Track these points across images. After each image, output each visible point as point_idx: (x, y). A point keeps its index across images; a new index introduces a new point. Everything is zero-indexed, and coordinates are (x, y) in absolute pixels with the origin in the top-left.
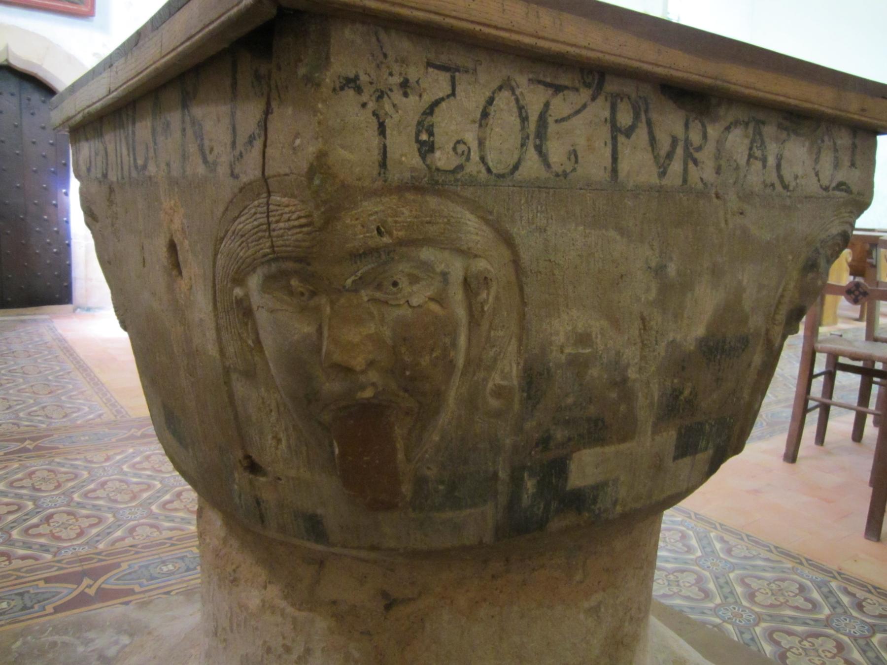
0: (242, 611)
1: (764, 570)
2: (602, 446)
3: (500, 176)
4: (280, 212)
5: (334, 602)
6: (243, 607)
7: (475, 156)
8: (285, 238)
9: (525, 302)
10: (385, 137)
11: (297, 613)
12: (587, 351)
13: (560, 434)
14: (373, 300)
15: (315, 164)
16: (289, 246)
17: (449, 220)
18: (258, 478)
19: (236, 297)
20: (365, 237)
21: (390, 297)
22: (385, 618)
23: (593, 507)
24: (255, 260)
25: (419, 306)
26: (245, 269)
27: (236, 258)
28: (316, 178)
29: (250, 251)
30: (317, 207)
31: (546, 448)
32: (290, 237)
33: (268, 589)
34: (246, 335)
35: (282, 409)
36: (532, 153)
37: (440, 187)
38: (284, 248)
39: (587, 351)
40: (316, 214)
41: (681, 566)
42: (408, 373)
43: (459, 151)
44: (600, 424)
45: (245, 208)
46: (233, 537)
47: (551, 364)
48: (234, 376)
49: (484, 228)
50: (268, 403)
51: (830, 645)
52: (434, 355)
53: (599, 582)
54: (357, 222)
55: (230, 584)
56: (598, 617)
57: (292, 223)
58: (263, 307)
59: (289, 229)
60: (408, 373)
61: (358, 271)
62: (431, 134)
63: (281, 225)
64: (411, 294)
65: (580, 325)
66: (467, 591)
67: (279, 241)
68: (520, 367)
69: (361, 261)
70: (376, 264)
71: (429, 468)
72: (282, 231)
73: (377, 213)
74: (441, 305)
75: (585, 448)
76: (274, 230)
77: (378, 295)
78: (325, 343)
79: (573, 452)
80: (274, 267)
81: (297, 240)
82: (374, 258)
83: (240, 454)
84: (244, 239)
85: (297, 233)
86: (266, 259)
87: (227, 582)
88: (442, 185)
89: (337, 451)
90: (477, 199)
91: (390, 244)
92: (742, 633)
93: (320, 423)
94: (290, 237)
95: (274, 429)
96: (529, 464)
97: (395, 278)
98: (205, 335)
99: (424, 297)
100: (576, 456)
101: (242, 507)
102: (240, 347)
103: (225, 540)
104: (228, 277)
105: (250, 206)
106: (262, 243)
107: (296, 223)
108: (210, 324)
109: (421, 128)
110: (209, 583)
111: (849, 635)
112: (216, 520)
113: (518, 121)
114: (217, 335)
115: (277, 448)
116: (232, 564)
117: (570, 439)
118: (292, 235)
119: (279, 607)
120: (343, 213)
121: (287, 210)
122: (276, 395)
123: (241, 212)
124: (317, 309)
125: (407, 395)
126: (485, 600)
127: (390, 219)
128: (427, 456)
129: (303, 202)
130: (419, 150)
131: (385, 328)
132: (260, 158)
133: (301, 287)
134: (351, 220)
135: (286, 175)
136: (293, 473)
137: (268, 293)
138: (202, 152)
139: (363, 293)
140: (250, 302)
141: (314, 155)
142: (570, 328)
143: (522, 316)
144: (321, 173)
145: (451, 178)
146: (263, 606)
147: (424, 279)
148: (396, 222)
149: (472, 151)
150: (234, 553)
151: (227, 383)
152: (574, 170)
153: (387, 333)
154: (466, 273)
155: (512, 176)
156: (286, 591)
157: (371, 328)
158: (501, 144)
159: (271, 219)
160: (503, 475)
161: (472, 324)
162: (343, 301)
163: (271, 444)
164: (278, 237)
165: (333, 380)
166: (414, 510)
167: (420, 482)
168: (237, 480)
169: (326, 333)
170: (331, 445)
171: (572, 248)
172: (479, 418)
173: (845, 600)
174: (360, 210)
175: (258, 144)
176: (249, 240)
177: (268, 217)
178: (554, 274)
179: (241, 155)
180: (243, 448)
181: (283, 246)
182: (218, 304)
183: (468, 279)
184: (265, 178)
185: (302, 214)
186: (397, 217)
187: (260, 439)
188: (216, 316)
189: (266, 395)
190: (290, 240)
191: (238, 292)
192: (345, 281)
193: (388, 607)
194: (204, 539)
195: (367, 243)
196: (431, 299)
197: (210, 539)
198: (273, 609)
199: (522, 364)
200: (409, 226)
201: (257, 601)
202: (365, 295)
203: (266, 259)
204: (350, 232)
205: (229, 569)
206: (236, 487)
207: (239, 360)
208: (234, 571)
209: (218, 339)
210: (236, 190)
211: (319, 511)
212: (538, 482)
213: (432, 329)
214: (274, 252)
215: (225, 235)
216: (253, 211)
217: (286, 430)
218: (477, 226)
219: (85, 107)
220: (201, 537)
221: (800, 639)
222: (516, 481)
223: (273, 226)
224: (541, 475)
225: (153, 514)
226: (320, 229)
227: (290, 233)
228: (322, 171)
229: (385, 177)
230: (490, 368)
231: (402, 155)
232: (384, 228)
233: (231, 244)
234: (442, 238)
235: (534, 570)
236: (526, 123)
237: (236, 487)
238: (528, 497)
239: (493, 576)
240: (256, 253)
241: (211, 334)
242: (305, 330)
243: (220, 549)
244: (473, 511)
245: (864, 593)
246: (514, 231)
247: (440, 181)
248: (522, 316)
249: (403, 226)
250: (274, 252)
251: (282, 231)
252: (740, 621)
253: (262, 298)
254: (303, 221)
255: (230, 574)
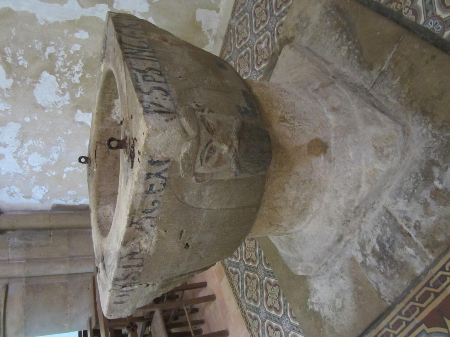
1: (235, 38)
41: (266, 331)
51: (257, 9)
111: (253, 5)
112: (56, 206)
173: (241, 10)
219: (93, 300)
221: (259, 56)
225: (287, 335)
245: (238, 4)
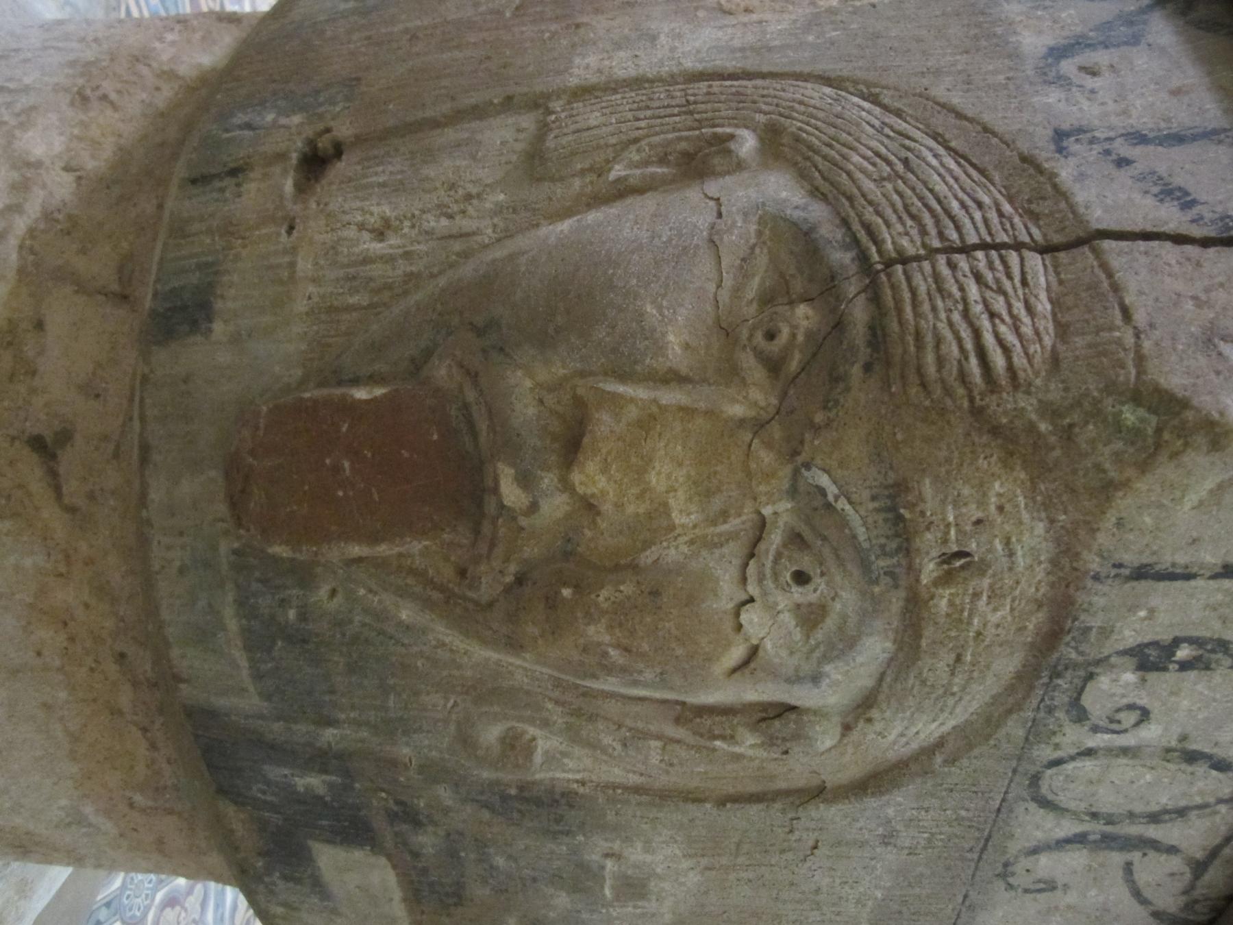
0: (18, 115)
1: (217, 906)
2: (405, 900)
3: (1035, 780)
4: (1007, 285)
5: (40, 325)
6: (27, 117)
7: (1094, 741)
8: (940, 303)
9: (724, 805)
10: (1214, 577)
11: (13, 242)
12: (607, 892)
13: (427, 841)
14: (762, 525)
15: (1189, 415)
16: (917, 315)
17: (953, 694)
18: (292, 173)
19: (732, 137)
20: (948, 525)
21: (769, 564)
22: (13, 439)
23: (278, 874)
24: (850, 199)
25: (739, 627)
26: (816, 167)
27: (838, 142)
28: (1141, 412)
29: (872, 185)
30: (1050, 411)
31: (392, 817)
32: (943, 316)
33: (64, 174)
34: (637, 158)
35: (457, 246)
36: (1068, 828)
37: (1045, 680)
38: (907, 295)
39: (607, 892)
40: (1027, 404)
42: (566, 592)
43: (1122, 716)
44: (451, 901)
45: (982, 172)
46: (177, 94)
47: (581, 838)
48: (528, 121)
49: (915, 746)
50: (470, 208)
52: (612, 652)
53: (135, 830)
54: (993, 508)
55: (76, 89)
56: (69, 824)
57: (985, 323)
58: (720, 215)
59: (966, 314)
60: (566, 592)
61: (850, 503)
62: (1184, 666)
63: (973, 291)
64: (773, 610)
65: (666, 885)
66: (87, 606)
67: (925, 280)
68: (575, 786)
69: (878, 510)
70: (866, 545)
71: (333, 593)
72: (955, 290)
73: (1011, 554)
74: (734, 670)
75: (397, 875)
76: (952, 266)
77: (775, 538)
78: (641, 393)
79: (389, 857)
80: (842, 258)
81: (939, 341)
82: (883, 541)
83: (344, 130)
84: (900, 167)
85: (959, 340)
86: (862, 235)
87: (80, 81)
88: (1047, 685)
89: (361, 394)
90: (992, 742)
91: (918, 581)
92: (108, 905)
93: (428, 354)
94: (943, 316)
95: (407, 223)
96: (357, 785)
97: (817, 580)
98: (618, 46)
99: (761, 636)
100: (383, 861)
101: (227, 131)
102: (602, 142)
103: (170, 75)
104: (781, 115)
105: (992, 188)
106: (904, 224)
107: (989, 339)
108: (650, 61)
109: (1209, 647)
110: (82, 40)
113: (1154, 808)
114: (625, 81)
115: (361, 227)
116: (119, 92)
117: (416, 855)
118: (951, 324)
119: (25, 200)
120: (1023, 475)
121: (1019, 308)
122: (489, 231)
123: (963, 157)
124: (731, 373)
125: (509, 579)
126: (72, 639)
127: (986, 582)
128: (362, 592)
129: (1055, 360)
130: (1155, 644)
131: (684, 548)
132: (1139, 225)
133: (794, 336)
134: (999, 495)
135: (1126, 313)
136: (304, 266)
137: (759, 233)
138: (1073, 45)
139: (785, 505)
140: (723, 174)
141: (1216, 416)
142: (659, 870)
143: (694, 797)
144: (1159, 431)
145: (1061, 699)
146: (28, 165)
147: (808, 637)
148: (976, 595)
149: (1115, 736)
150: (144, 96)
151: (508, 104)
152: (1010, 887)
153: (673, 553)
154: (807, 711)
155: (1029, 798)
156: (60, 217)
157: (685, 514)
158: (1112, 782)
159: (980, 254)
160: (329, 735)
161: (678, 707)
162: (766, 457)
163: (372, 214)
164: (937, 277)
165: (541, 401)
166: (235, 552)
167: (304, 575)
168: (283, 121)
169: (671, 397)
170: (373, 379)
171: (838, 881)
172: (455, 704)
174: (1025, 516)
175: (1171, 218)
176: (900, 182)
177: (984, 246)
178: (783, 851)
179: (1122, 162)
180: (359, 140)
181: (914, 292)
182: (703, 86)
183: (793, 716)
184: (1092, 238)
185: (1019, 360)
186: (989, 597)
187: (383, 185)
188: (672, 80)
189: (488, 205)
190: (936, 317)
191: (747, 144)
192: (824, 470)
193: (38, 444)
194: (172, 29)
195: (928, 529)
196: (754, 651)
197: (173, 43)
198: (22, 187)
199: (581, 790)
200: (961, 621)
201: (38, 151)
202: (780, 511)
203: (862, 235)
204: (966, 491)
205: (108, 87)
206: (270, 117)
207: (570, 138)
208: (104, 98)
209: (616, 82)
210: (1024, 146)
211: (219, 328)
212: (320, 798)
213: (680, 651)
214: (889, 264)
215: (885, 108)
216: (986, 200)
217: (407, 255)
218: (922, 736)
220: (179, 22)
222: (321, 760)
223: (962, 261)
224: (335, 804)
226: (977, 412)
227: (956, 317)
228: (1166, 436)
229: (1108, 577)
230: (573, 735)
231: (1152, 611)
232: (962, 567)
233: (873, 126)
234: (911, 682)
235: (145, 730)
236: (1145, 820)
237: (270, 117)
238: (286, 776)
239: (122, 656)
240: (870, 203)
241: (623, 65)
242: (671, 338)
243: (149, 66)
244: (245, 673)
246: (898, 797)
247: (1060, 681)
248: (694, 797)
249: (962, 611)
250: (889, 264)
251: (955, 290)
252: (128, 897)
253: (746, 215)
254: (998, 360)
255: (98, 87)
